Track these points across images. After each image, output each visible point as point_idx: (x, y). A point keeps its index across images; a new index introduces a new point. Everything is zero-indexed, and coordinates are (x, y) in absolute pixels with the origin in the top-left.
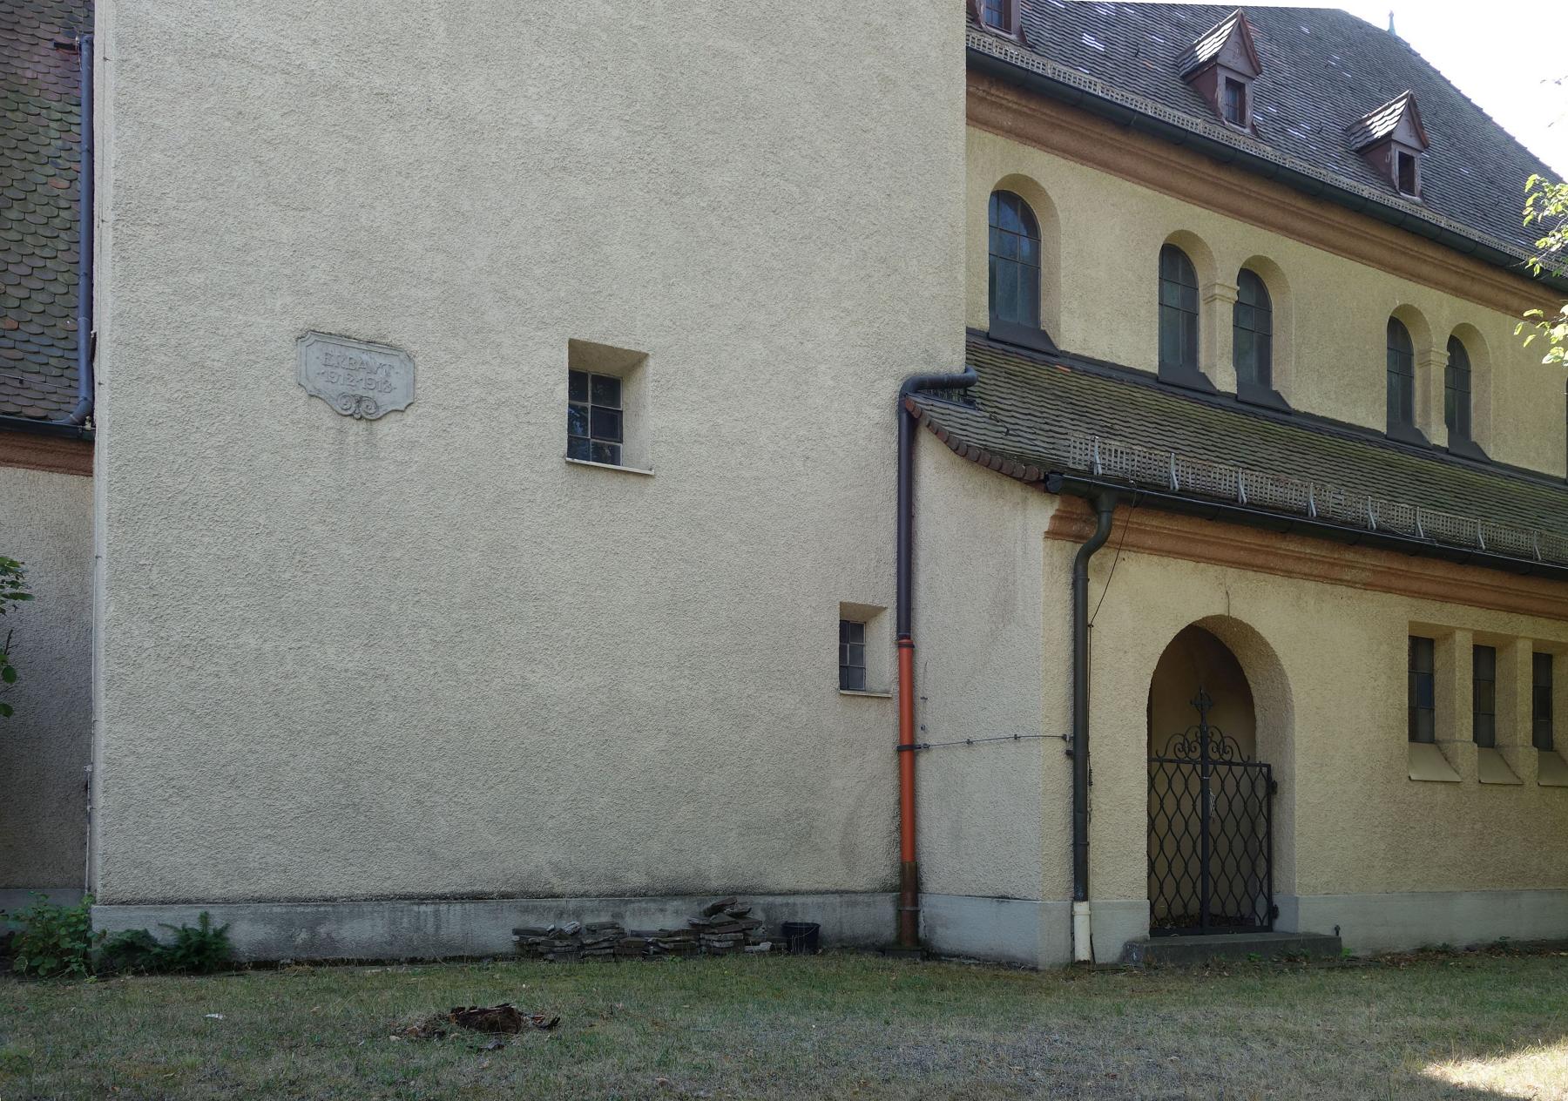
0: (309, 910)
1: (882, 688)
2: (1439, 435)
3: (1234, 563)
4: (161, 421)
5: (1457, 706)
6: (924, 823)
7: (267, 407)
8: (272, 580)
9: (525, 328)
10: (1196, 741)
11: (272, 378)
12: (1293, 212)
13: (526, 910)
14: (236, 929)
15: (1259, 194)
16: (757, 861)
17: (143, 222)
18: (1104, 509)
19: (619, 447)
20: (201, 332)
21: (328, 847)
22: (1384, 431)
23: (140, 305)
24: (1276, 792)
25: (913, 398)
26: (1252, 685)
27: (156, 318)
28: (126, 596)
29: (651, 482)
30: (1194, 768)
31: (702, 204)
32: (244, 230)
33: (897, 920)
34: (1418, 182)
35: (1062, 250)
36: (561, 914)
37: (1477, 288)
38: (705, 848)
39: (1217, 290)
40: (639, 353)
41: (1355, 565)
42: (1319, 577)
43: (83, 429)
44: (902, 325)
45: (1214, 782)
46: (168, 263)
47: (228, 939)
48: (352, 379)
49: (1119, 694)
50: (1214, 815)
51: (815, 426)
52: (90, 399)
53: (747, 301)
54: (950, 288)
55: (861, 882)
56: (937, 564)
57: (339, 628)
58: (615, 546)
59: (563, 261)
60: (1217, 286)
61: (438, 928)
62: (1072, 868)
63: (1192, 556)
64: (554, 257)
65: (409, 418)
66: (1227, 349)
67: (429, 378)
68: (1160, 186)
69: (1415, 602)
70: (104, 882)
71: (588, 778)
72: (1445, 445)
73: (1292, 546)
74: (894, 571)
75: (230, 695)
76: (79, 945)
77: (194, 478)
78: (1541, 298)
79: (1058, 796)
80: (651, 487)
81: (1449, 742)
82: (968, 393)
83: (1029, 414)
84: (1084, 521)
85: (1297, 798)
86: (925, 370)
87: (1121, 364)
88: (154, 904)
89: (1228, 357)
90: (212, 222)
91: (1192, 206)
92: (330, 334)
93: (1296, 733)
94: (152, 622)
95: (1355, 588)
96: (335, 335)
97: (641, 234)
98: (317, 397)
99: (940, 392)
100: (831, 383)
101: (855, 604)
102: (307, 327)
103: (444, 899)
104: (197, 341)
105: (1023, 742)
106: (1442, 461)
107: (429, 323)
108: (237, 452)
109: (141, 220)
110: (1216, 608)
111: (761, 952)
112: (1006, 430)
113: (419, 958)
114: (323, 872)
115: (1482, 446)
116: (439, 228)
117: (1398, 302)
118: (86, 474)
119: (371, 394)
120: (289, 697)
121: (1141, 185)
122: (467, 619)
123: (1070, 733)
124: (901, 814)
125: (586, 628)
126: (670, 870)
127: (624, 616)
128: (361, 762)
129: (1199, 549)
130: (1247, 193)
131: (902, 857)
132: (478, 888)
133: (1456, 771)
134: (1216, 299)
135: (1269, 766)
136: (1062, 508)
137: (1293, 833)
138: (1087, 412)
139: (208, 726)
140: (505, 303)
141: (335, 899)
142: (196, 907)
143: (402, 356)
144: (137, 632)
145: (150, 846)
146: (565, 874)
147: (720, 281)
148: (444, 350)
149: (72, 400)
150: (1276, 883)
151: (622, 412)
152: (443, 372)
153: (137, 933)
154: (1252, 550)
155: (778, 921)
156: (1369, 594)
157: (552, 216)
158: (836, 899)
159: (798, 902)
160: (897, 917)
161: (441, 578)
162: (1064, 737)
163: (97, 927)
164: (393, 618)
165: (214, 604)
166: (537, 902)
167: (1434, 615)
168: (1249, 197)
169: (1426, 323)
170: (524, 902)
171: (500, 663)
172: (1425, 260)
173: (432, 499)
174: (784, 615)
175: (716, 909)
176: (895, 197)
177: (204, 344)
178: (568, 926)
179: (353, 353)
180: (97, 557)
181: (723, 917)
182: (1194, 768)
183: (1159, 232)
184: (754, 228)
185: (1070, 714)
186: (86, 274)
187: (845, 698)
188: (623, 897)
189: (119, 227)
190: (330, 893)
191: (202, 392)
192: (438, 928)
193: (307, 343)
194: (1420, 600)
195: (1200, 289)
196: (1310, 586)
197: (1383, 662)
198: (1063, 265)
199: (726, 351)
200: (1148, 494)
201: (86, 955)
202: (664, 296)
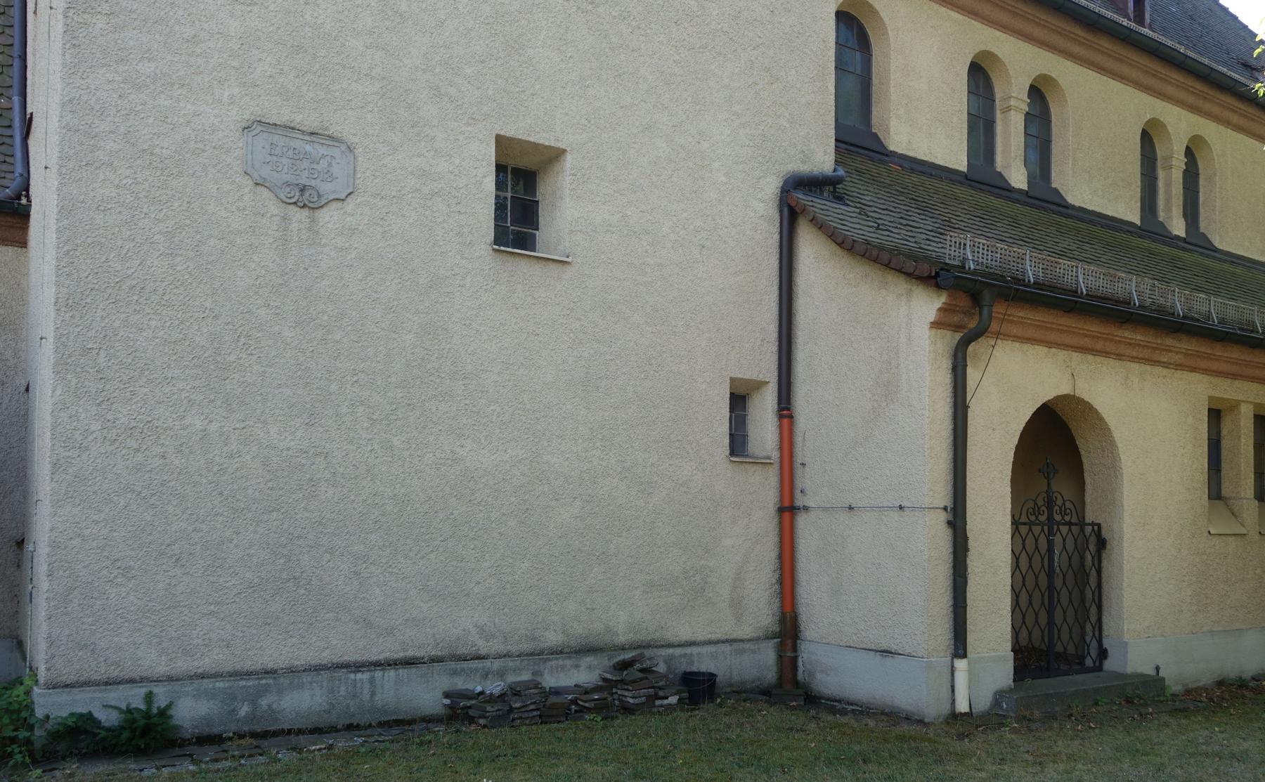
0: (250, 683)
1: (765, 454)
2: (1178, 228)
3: (1078, 348)
4: (109, 207)
5: (1242, 468)
6: (803, 576)
7: (214, 194)
8: (218, 362)
9: (456, 124)
10: (1044, 505)
11: (219, 167)
12: (1072, 38)
13: (454, 673)
14: (180, 706)
15: (1047, 22)
16: (659, 616)
17: (94, 11)
18: (985, 303)
19: (535, 234)
20: (151, 120)
21: (269, 621)
22: (1138, 222)
23: (91, 92)
24: (1105, 548)
25: (796, 195)
26: (1083, 452)
27: (106, 106)
28: (74, 379)
29: (568, 267)
30: (1043, 530)
31: (614, 14)
32: (194, 22)
33: (778, 664)
34: (1147, 16)
35: (892, 65)
36: (486, 676)
37: (1207, 106)
38: (614, 606)
39: (1012, 102)
40: (558, 149)
41: (1172, 348)
42: (1143, 359)
43: (19, 204)
44: (783, 128)
45: (1058, 539)
46: (119, 52)
47: (171, 717)
48: (295, 168)
49: (989, 467)
50: (1058, 570)
51: (710, 218)
52: (25, 175)
53: (652, 104)
54: (822, 96)
55: (746, 631)
56: (816, 344)
57: (281, 409)
58: (537, 328)
59: (491, 62)
60: (1012, 99)
61: (373, 694)
62: (952, 627)
63: (1047, 342)
64: (483, 58)
65: (350, 205)
66: (1020, 152)
67: (368, 169)
68: (969, 13)
69: (1212, 379)
70: (48, 665)
71: (511, 544)
72: (1183, 235)
73: (1126, 333)
74: (775, 348)
75: (175, 475)
76: (23, 734)
77: (142, 263)
78: (1255, 115)
79: (940, 562)
80: (569, 272)
81: (1234, 499)
82: (837, 190)
83: (887, 209)
84: (965, 313)
85: (1125, 554)
86: (802, 169)
87: (938, 163)
88: (97, 685)
89: (1020, 159)
90: (163, 13)
91: (994, 30)
92: (276, 125)
93: (1125, 497)
94: (99, 405)
95: (1169, 368)
96: (280, 126)
97: (560, 39)
98: (262, 185)
99: (813, 189)
100: (723, 179)
101: (742, 379)
102: (253, 117)
103: (379, 666)
104: (146, 129)
105: (907, 512)
106: (1184, 249)
107: (369, 116)
108: (184, 237)
109: (92, 9)
110: (1065, 389)
111: (670, 708)
112: (876, 225)
113: (355, 724)
114: (264, 646)
115: (1209, 236)
116: (378, 27)
117: (1148, 116)
118: (21, 245)
119: (313, 183)
120: (233, 476)
121: (955, 11)
122: (402, 397)
123: (950, 505)
124: (781, 567)
125: (510, 404)
126: (586, 627)
127: (543, 392)
128: (301, 537)
129: (1053, 337)
130: (1037, 20)
131: (782, 607)
132: (410, 653)
133: (1242, 525)
134: (1010, 110)
135: (1099, 525)
136: (948, 302)
137: (1122, 585)
138: (927, 207)
139: (153, 506)
140: (438, 99)
141: (276, 671)
142: (140, 687)
143: (343, 147)
144: (83, 415)
145: (94, 628)
146: (489, 636)
147: (630, 85)
148: (383, 143)
149: (8, 175)
150: (1105, 627)
151: (537, 202)
152: (381, 163)
153: (81, 715)
154: (1094, 337)
155: (677, 671)
156: (1179, 374)
157: (482, 20)
158: (727, 648)
159: (694, 653)
160: (778, 661)
161: (378, 359)
162: (945, 509)
163: (40, 713)
164: (333, 397)
165: (160, 386)
166: (465, 665)
167: (1227, 390)
168: (1038, 24)
169: (1169, 134)
170: (453, 665)
171: (431, 438)
172: (1171, 82)
173: (370, 284)
174: (683, 389)
175: (625, 665)
176: (777, 13)
177: (153, 132)
178: (494, 687)
179: (297, 144)
180: (41, 339)
181: (632, 674)
182: (1043, 530)
183: (967, 51)
184: (659, 37)
185: (950, 487)
186: (20, 56)
187: (734, 464)
188: (540, 655)
189: (70, 14)
190: (270, 666)
191: (151, 179)
192: (373, 694)
193: (254, 133)
194: (1217, 378)
195: (997, 101)
196: (1136, 367)
197: (1189, 432)
198: (892, 77)
199: (635, 148)
200: (1023, 290)
201: (28, 742)
202: (581, 97)
